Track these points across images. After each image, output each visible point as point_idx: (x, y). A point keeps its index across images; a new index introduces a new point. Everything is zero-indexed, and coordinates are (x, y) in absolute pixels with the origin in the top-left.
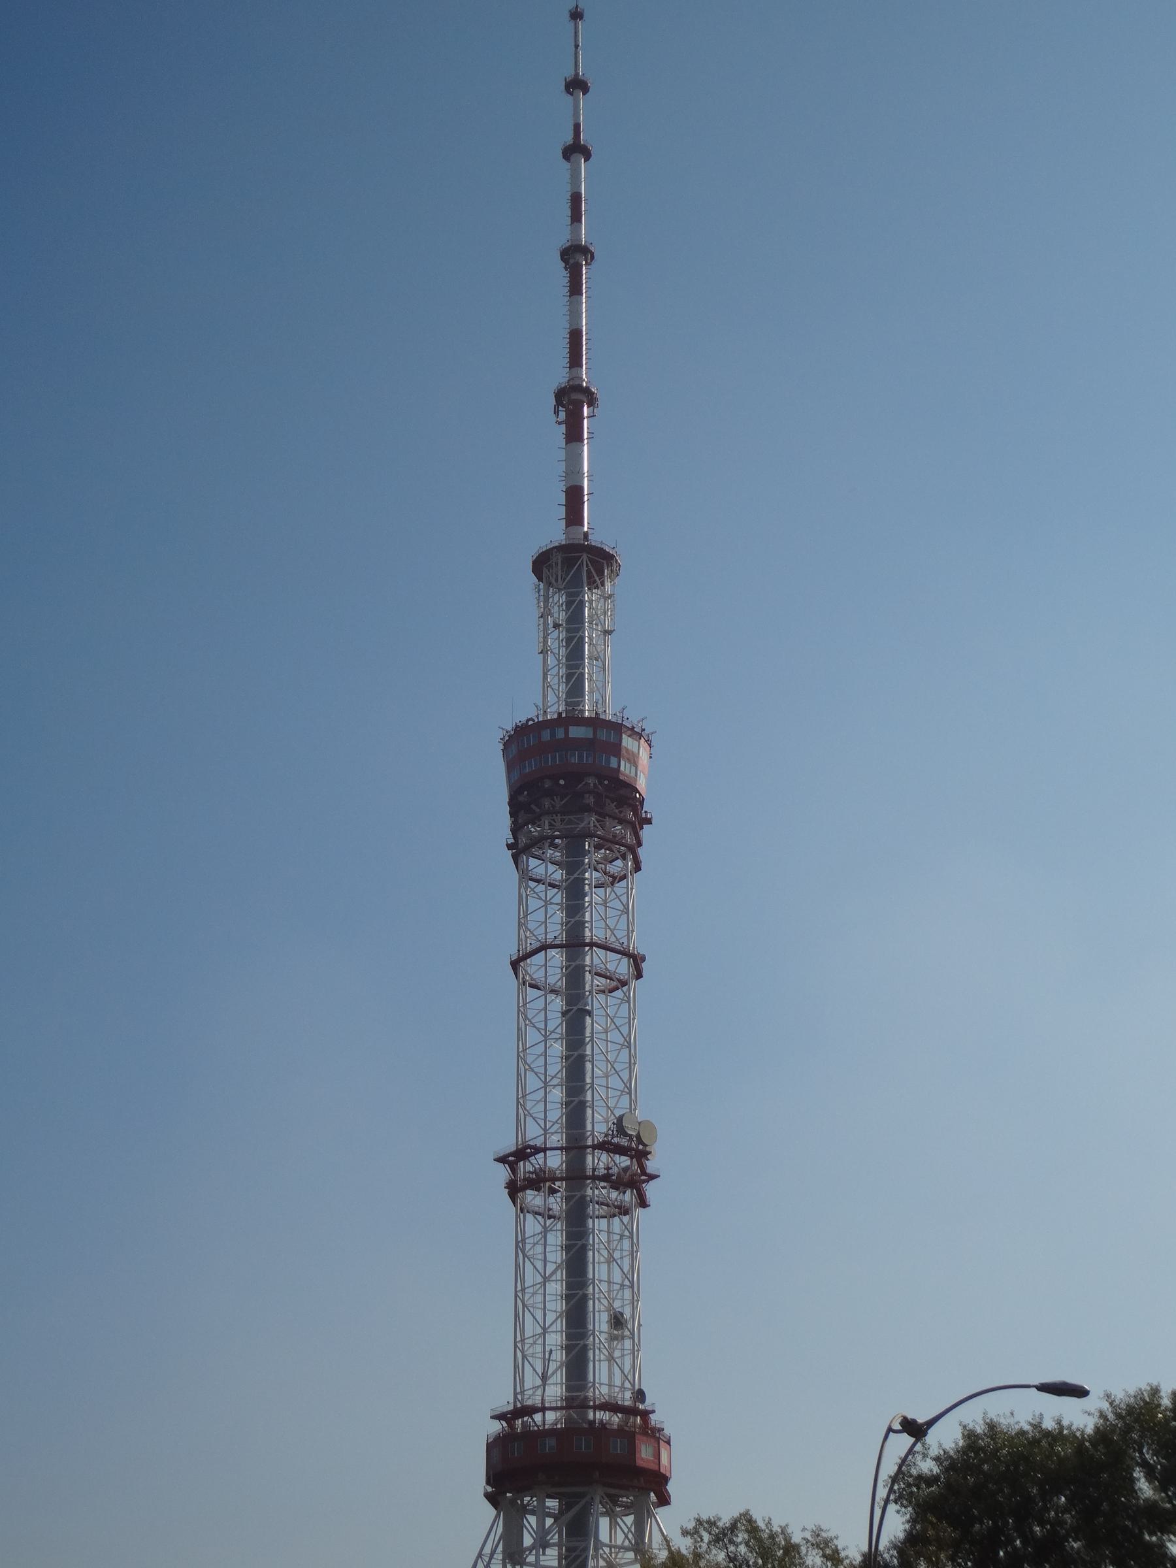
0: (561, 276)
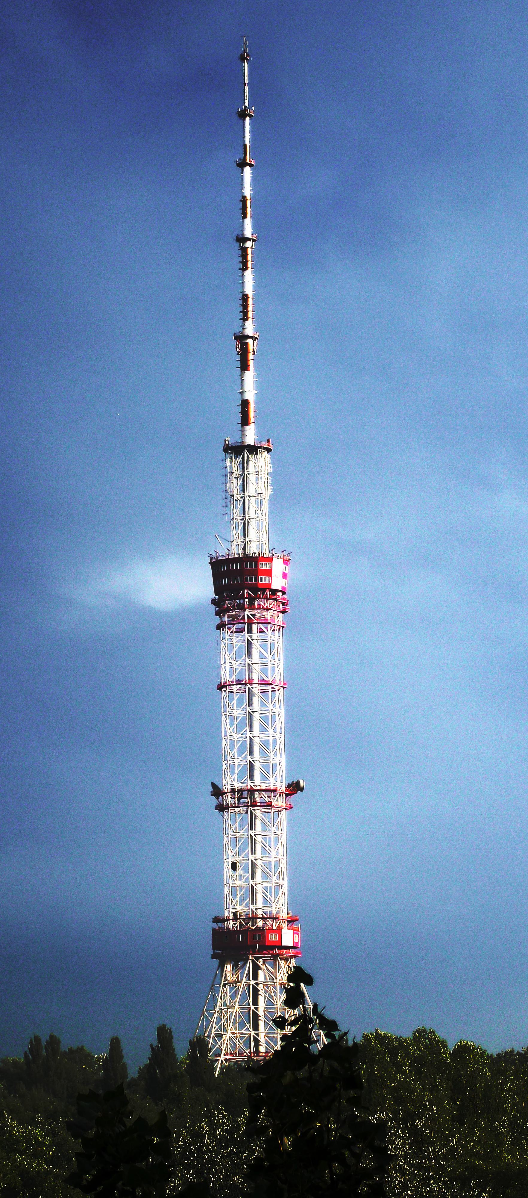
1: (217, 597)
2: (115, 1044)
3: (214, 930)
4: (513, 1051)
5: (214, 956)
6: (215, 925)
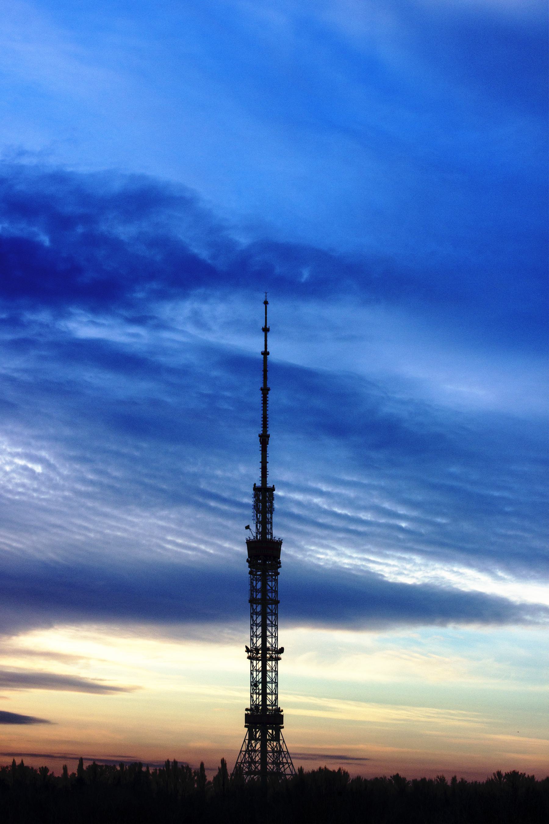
3: (246, 714)
5: (246, 726)
6: (246, 712)
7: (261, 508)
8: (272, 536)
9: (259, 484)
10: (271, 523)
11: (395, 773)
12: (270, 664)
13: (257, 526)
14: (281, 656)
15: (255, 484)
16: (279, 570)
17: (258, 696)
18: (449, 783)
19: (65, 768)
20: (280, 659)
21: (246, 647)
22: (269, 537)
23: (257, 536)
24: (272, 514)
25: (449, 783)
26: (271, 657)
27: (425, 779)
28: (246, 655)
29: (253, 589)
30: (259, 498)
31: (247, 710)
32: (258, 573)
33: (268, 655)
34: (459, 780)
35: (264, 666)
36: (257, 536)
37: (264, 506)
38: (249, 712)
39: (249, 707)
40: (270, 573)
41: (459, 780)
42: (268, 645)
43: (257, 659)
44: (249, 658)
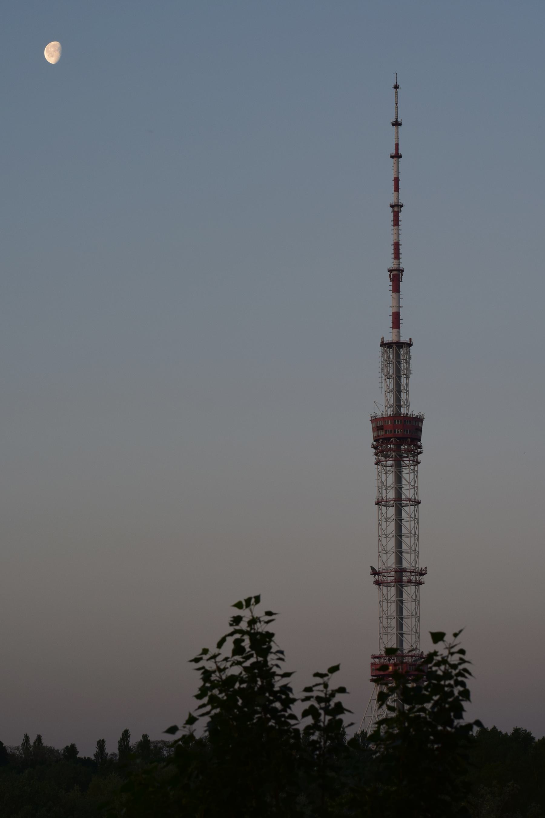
0: (389, 284)
1: (375, 443)
2: (411, 339)
3: (372, 664)
4: (374, 447)
6: (373, 661)
7: (392, 370)
8: (408, 409)
9: (390, 336)
10: (407, 391)
11: (198, 690)
12: (408, 591)
13: (386, 396)
14: (424, 578)
15: (383, 338)
16: (420, 457)
17: (389, 636)
18: (364, 712)
19: (101, 744)
20: (420, 583)
21: (372, 568)
22: (404, 411)
23: (386, 411)
24: (408, 377)
25: (364, 712)
26: (410, 581)
27: (67, 746)
28: (372, 579)
29: (382, 486)
30: (388, 357)
31: (374, 657)
32: (388, 462)
33: (404, 578)
34: (134, 740)
35: (400, 594)
36: (386, 411)
37: (398, 370)
38: (376, 660)
39: (377, 653)
40: (407, 462)
41: (206, 728)
42: (405, 564)
43: (387, 584)
44: (377, 583)
